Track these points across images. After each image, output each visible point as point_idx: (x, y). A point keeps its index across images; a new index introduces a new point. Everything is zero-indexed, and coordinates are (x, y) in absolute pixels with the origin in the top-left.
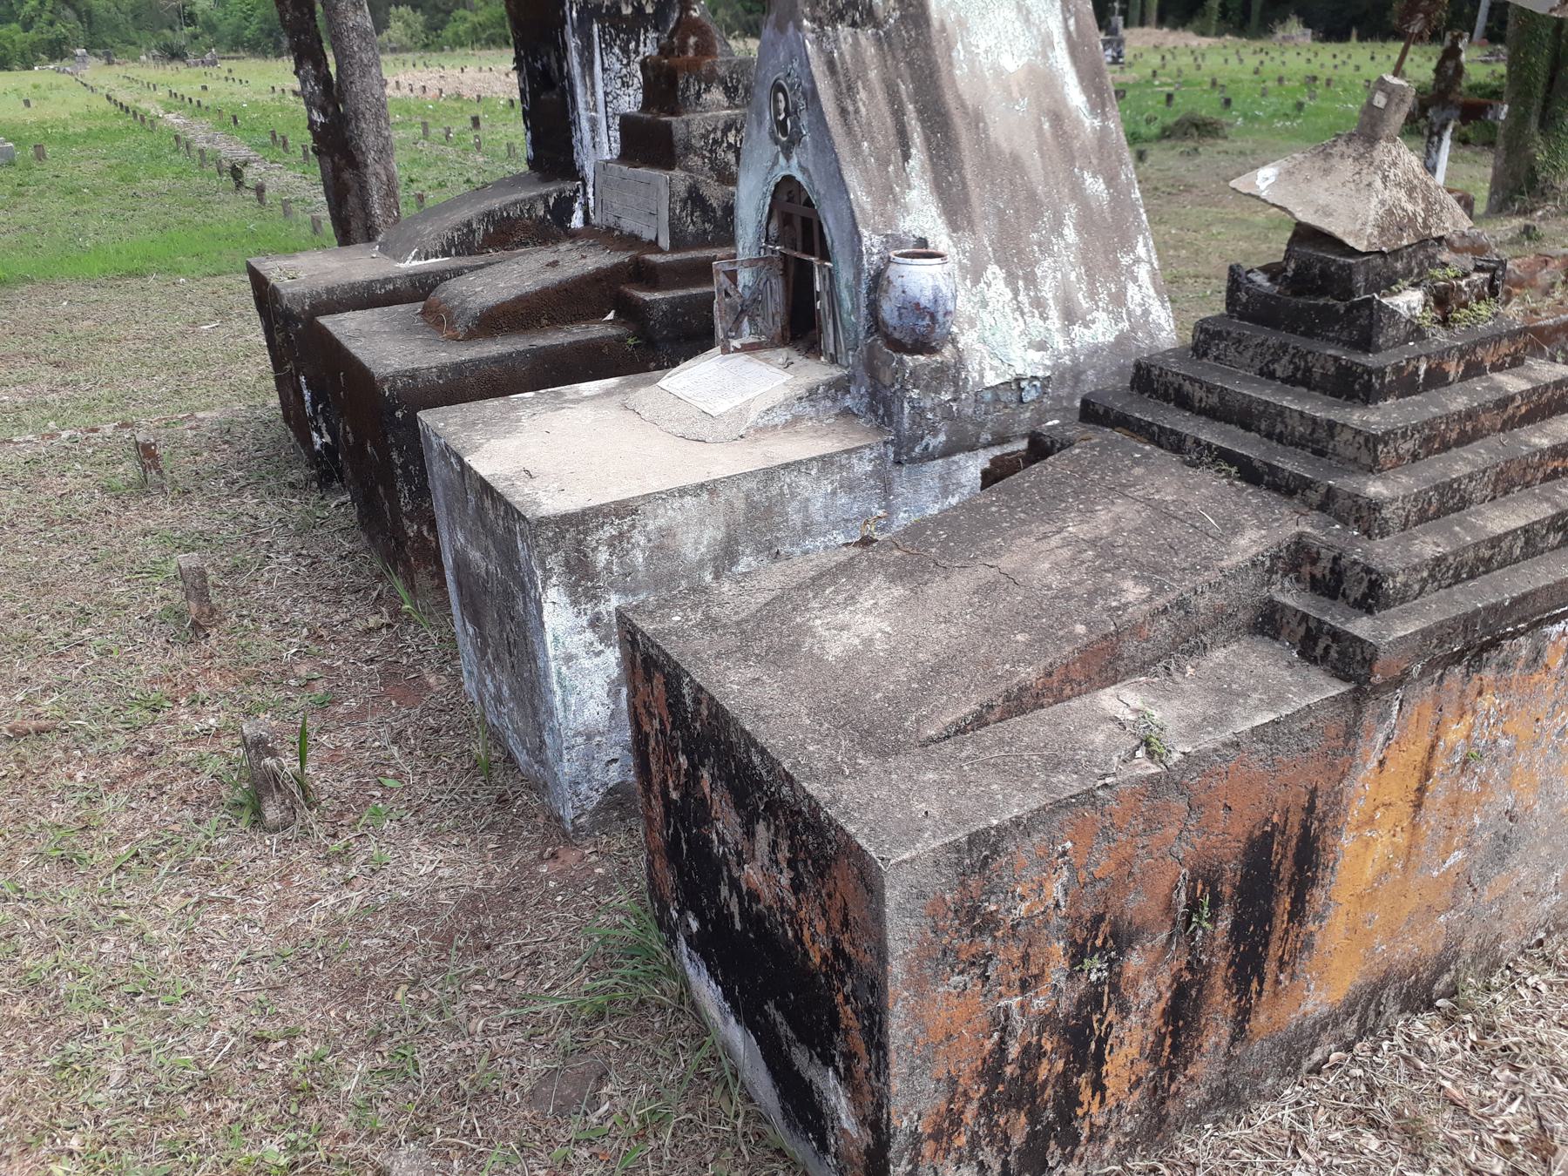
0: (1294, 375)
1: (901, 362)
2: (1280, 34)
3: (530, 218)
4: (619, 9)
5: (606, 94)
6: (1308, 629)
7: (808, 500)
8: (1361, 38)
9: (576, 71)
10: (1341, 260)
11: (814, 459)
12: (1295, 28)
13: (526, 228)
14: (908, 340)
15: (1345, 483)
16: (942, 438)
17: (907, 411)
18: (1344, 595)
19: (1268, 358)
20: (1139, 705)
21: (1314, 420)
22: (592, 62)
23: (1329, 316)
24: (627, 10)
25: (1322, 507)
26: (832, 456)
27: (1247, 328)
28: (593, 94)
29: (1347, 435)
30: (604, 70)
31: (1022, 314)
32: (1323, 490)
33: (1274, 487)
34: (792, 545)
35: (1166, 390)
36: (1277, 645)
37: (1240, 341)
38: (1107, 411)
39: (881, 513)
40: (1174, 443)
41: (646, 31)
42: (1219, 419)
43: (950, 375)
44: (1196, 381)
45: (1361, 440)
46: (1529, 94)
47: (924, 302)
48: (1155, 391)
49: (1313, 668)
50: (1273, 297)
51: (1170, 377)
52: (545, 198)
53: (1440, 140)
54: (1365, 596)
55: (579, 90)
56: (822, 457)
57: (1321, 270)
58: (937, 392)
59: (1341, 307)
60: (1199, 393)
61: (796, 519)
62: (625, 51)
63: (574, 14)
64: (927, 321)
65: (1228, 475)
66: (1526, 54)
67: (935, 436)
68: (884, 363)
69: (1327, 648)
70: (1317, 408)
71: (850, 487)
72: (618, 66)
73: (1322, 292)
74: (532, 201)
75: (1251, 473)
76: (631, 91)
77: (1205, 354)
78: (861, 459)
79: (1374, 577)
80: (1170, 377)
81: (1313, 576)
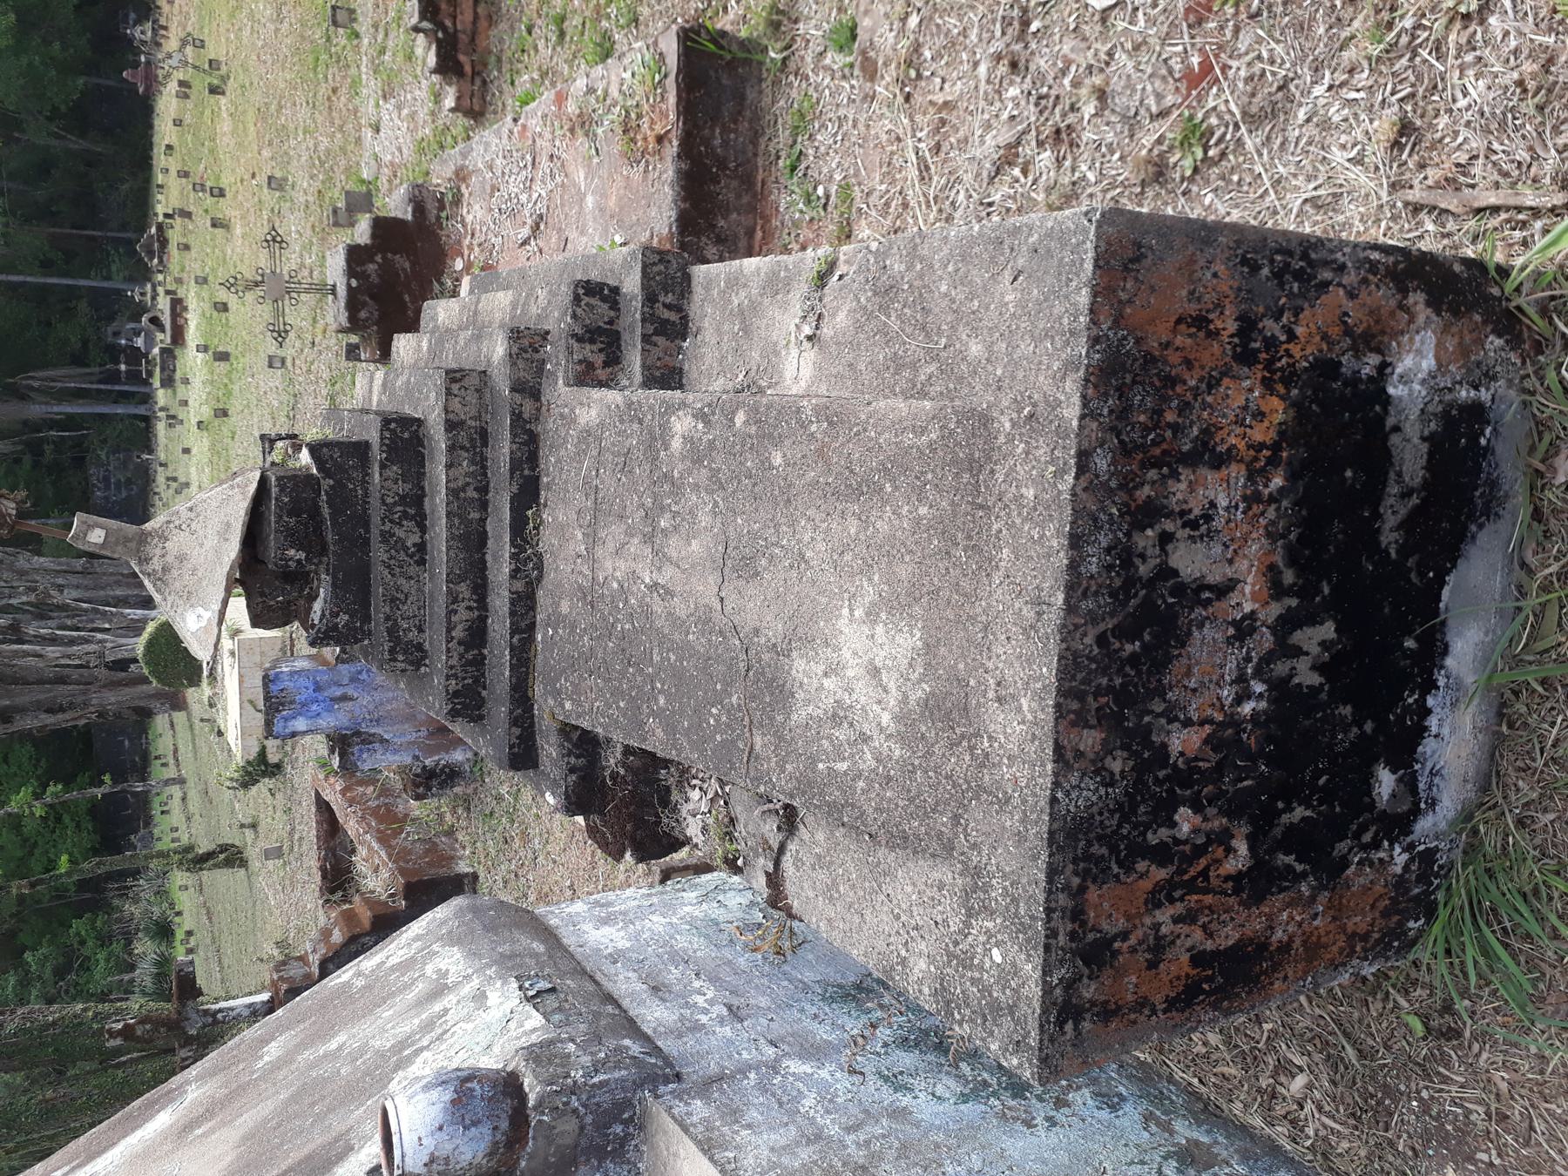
0: (412, 518)
1: (539, 1106)
6: (656, 333)
7: (772, 1149)
10: (274, 491)
11: (711, 1159)
14: (507, 1105)
15: (502, 384)
16: (627, 1042)
17: (603, 1077)
18: (611, 322)
19: (402, 556)
20: (794, 352)
21: (451, 449)
23: (340, 498)
25: (536, 395)
26: (698, 1143)
27: (379, 610)
29: (455, 404)
31: (446, 1032)
32: (518, 397)
33: (533, 459)
34: (845, 1147)
35: (470, 663)
36: (686, 367)
37: (393, 600)
38: (515, 722)
39: (752, 1075)
40: (524, 603)
42: (485, 578)
43: (538, 1054)
44: (449, 621)
45: (455, 387)
47: (448, 1095)
48: (476, 681)
49: (691, 314)
50: (334, 577)
51: (454, 662)
53: (220, 1010)
54: (604, 299)
56: (704, 1151)
57: (290, 515)
58: (569, 1056)
59: (327, 483)
60: (463, 615)
61: (805, 1154)
64: (474, 1085)
65: (538, 514)
67: (627, 1048)
68: (550, 1141)
69: (668, 306)
70: (438, 474)
71: (733, 1114)
73: (315, 512)
75: (528, 494)
77: (420, 647)
78: (689, 1114)
79: (581, 291)
80: (454, 662)
81: (606, 364)
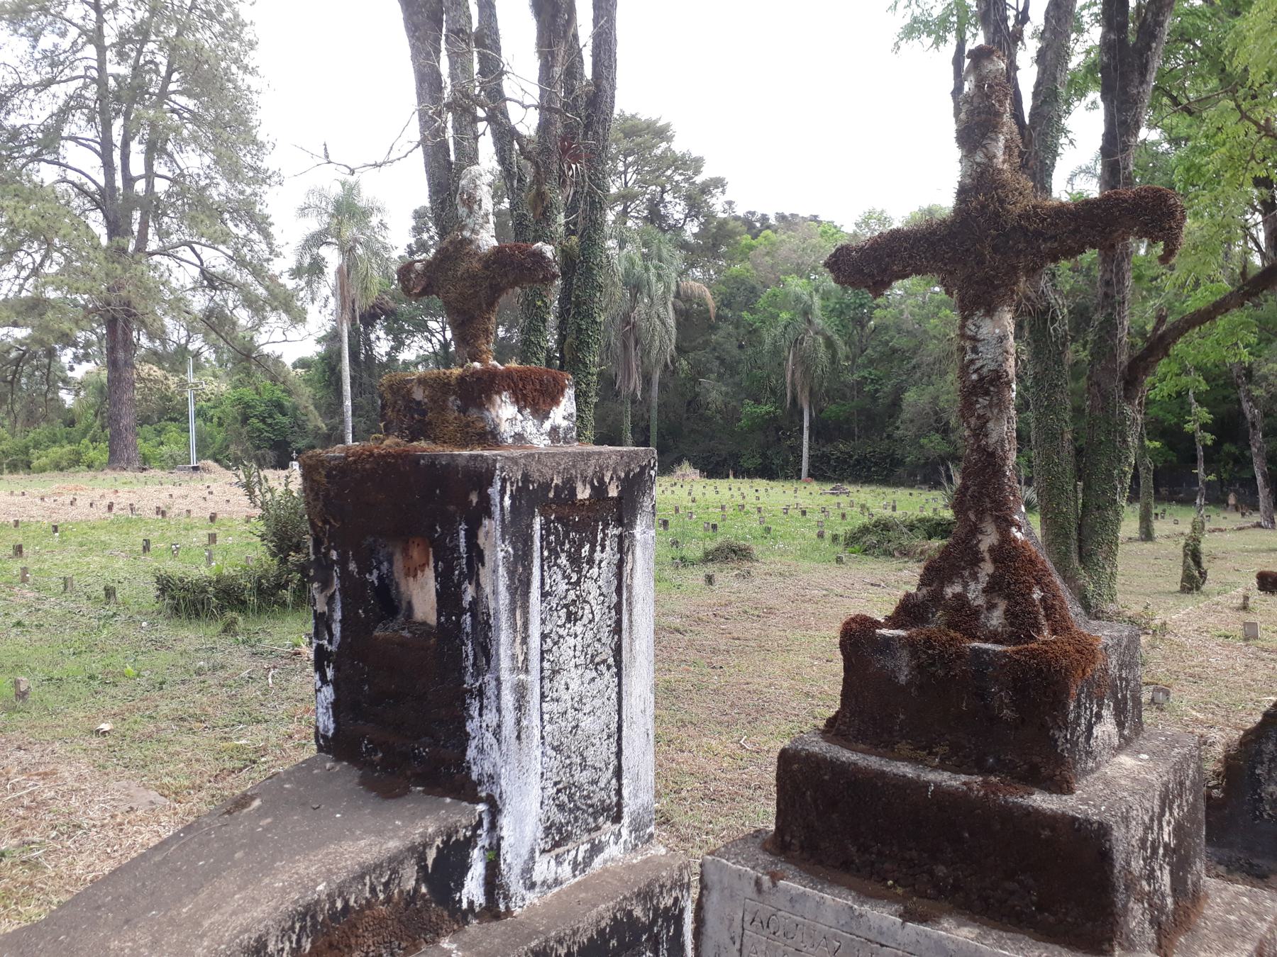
2: (679, 473)
3: (389, 899)
4: (573, 492)
5: (544, 637)
8: (735, 476)
9: (500, 601)
12: (686, 468)
13: (381, 921)
22: (527, 584)
24: (583, 493)
28: (524, 641)
30: (544, 595)
41: (606, 526)
46: (1067, 536)
52: (418, 852)
55: (504, 637)
62: (575, 560)
63: (507, 502)
66: (1058, 504)
72: (563, 586)
74: (395, 863)
76: (579, 628)
